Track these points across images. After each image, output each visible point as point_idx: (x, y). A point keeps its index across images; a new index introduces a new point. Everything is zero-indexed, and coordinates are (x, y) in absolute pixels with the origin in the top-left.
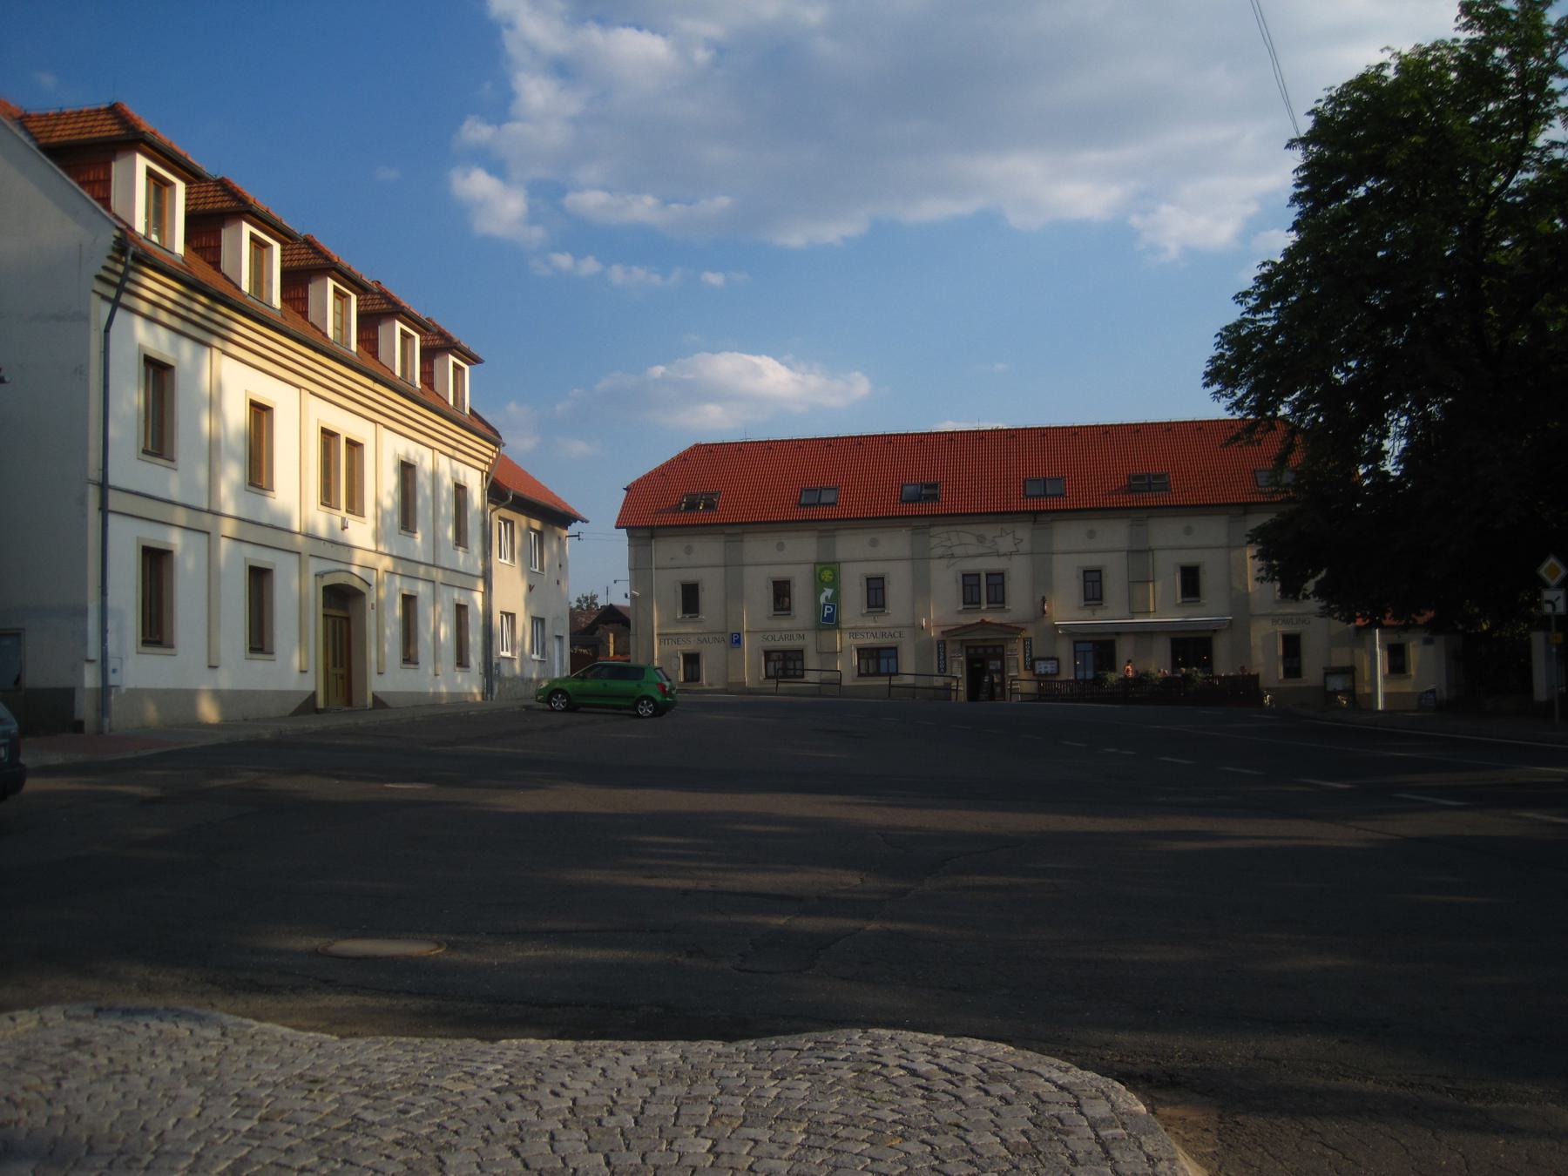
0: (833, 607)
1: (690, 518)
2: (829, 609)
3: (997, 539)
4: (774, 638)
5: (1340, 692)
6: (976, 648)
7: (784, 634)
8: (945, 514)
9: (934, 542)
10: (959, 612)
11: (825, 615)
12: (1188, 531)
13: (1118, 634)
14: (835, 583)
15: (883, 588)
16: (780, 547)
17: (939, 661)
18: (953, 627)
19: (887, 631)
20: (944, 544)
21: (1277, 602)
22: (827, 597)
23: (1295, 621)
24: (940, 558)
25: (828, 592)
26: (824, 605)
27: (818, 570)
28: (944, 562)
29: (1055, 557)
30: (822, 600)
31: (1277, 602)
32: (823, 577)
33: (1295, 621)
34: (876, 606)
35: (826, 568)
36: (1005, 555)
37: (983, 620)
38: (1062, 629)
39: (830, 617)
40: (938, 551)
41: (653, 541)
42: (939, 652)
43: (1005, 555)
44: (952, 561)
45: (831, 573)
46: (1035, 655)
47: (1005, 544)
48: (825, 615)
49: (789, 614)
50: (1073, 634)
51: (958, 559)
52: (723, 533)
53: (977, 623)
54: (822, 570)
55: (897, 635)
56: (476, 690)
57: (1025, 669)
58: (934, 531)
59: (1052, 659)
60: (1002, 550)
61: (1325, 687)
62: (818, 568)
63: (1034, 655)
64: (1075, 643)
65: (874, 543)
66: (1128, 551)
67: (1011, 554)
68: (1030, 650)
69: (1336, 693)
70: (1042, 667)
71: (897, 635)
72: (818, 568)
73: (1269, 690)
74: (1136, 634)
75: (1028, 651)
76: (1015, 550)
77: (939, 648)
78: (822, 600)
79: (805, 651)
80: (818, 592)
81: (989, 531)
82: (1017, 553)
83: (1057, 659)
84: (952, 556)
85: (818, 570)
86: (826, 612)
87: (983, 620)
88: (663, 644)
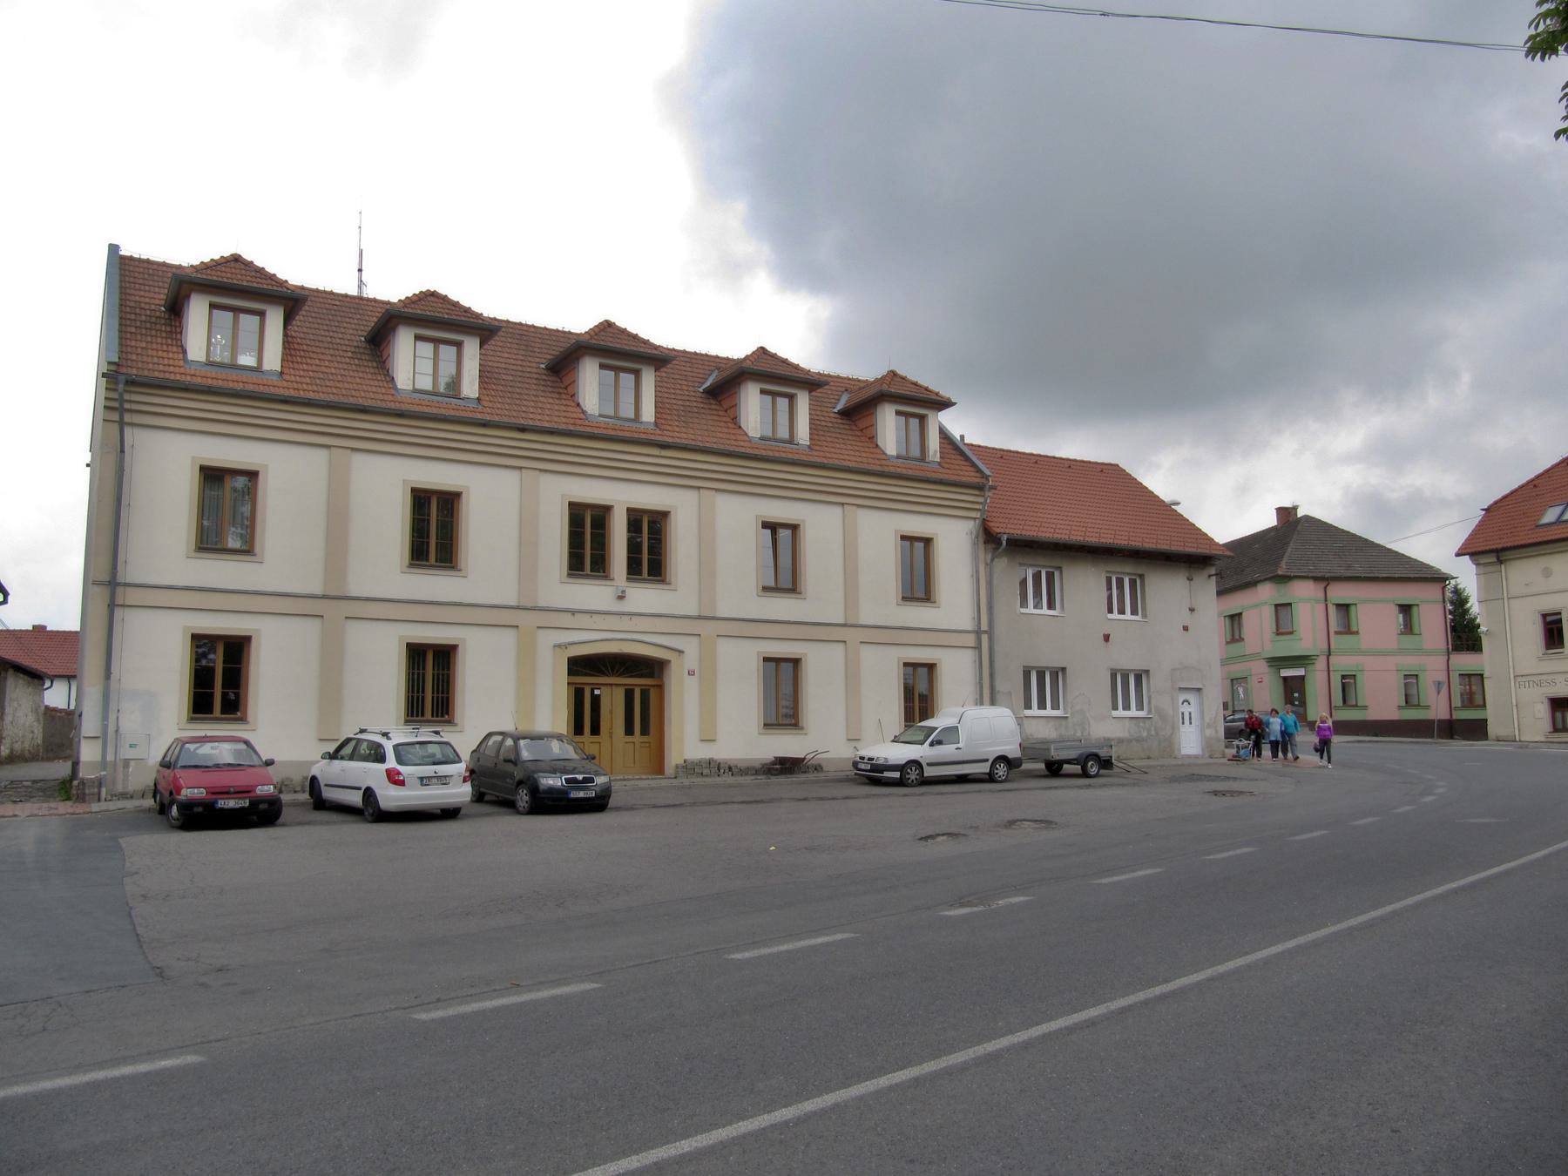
41: (1503, 566)
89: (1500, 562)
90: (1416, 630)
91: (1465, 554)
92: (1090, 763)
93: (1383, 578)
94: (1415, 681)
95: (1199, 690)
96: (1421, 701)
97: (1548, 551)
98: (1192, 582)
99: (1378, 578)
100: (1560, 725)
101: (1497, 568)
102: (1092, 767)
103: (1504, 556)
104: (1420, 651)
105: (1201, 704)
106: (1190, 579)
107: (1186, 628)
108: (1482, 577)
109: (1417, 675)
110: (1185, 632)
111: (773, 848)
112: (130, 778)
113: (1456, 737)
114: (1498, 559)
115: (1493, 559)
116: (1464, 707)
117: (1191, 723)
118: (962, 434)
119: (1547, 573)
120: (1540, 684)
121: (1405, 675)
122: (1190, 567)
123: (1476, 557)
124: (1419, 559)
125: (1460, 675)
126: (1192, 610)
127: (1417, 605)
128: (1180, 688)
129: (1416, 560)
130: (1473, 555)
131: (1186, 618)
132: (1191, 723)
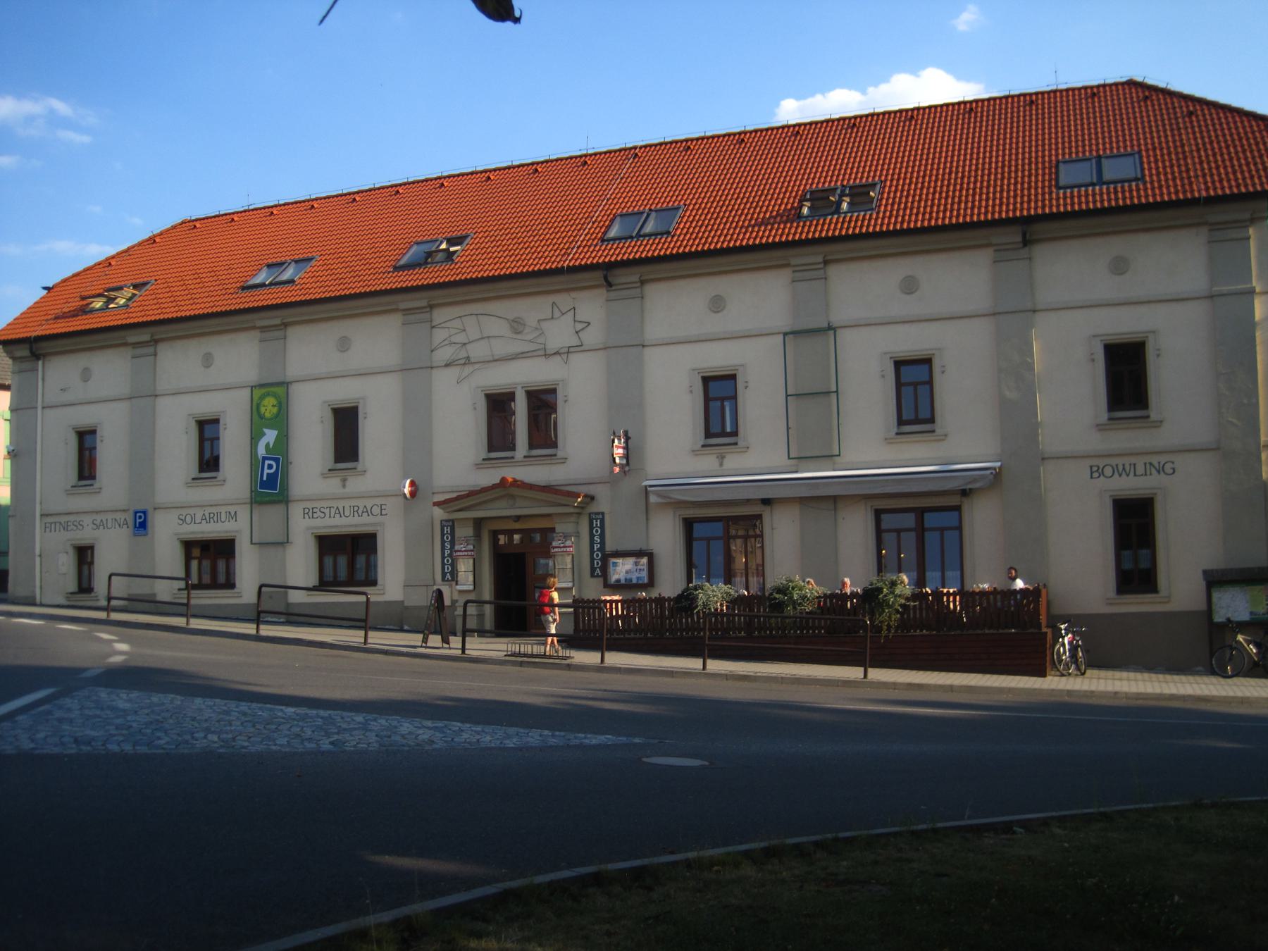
0: (277, 460)
1: (829, 226)
2: (270, 467)
3: (545, 325)
4: (340, 513)
5: (1242, 626)
6: (510, 533)
7: (208, 510)
8: (965, 223)
9: (439, 335)
10: (478, 466)
11: (265, 478)
12: (909, 286)
13: (767, 502)
14: (282, 421)
15: (930, 383)
16: (208, 360)
17: (443, 558)
18: (454, 495)
19: (361, 503)
20: (454, 339)
21: (1100, 427)
22: (267, 445)
23: (1140, 470)
24: (447, 365)
25: (270, 436)
26: (264, 459)
27: (256, 398)
28: (453, 372)
29: (647, 351)
30: (261, 451)
31: (1100, 427)
32: (263, 410)
33: (1140, 470)
34: (724, 434)
35: (268, 394)
36: (557, 353)
37: (503, 480)
38: (658, 494)
39: (271, 482)
40: (444, 354)
41: (40, 363)
42: (443, 542)
43: (557, 353)
44: (468, 369)
45: (275, 403)
46: (609, 547)
47: (559, 333)
48: (265, 478)
49: (736, 444)
50: (679, 504)
51: (477, 366)
52: (126, 344)
53: (494, 487)
54: (262, 398)
55: (376, 510)
56: (541, 572)
57: (592, 575)
58: (440, 315)
59: (638, 554)
60: (553, 345)
61: (1209, 611)
62: (257, 393)
63: (609, 547)
64: (878, 513)
65: (344, 345)
66: (785, 334)
67: (569, 351)
68: (602, 536)
69: (1233, 627)
70: (622, 569)
71: (376, 510)
72: (257, 393)
73: (1074, 621)
74: (803, 501)
75: (597, 539)
76: (575, 342)
77: (443, 535)
78: (261, 451)
79: (96, 548)
80: (255, 438)
81: (531, 309)
82: (579, 348)
83: (651, 556)
84: (468, 361)
85: (256, 398)
86: (266, 471)
87: (503, 480)
88: (48, 530)
120: (1096, 472)
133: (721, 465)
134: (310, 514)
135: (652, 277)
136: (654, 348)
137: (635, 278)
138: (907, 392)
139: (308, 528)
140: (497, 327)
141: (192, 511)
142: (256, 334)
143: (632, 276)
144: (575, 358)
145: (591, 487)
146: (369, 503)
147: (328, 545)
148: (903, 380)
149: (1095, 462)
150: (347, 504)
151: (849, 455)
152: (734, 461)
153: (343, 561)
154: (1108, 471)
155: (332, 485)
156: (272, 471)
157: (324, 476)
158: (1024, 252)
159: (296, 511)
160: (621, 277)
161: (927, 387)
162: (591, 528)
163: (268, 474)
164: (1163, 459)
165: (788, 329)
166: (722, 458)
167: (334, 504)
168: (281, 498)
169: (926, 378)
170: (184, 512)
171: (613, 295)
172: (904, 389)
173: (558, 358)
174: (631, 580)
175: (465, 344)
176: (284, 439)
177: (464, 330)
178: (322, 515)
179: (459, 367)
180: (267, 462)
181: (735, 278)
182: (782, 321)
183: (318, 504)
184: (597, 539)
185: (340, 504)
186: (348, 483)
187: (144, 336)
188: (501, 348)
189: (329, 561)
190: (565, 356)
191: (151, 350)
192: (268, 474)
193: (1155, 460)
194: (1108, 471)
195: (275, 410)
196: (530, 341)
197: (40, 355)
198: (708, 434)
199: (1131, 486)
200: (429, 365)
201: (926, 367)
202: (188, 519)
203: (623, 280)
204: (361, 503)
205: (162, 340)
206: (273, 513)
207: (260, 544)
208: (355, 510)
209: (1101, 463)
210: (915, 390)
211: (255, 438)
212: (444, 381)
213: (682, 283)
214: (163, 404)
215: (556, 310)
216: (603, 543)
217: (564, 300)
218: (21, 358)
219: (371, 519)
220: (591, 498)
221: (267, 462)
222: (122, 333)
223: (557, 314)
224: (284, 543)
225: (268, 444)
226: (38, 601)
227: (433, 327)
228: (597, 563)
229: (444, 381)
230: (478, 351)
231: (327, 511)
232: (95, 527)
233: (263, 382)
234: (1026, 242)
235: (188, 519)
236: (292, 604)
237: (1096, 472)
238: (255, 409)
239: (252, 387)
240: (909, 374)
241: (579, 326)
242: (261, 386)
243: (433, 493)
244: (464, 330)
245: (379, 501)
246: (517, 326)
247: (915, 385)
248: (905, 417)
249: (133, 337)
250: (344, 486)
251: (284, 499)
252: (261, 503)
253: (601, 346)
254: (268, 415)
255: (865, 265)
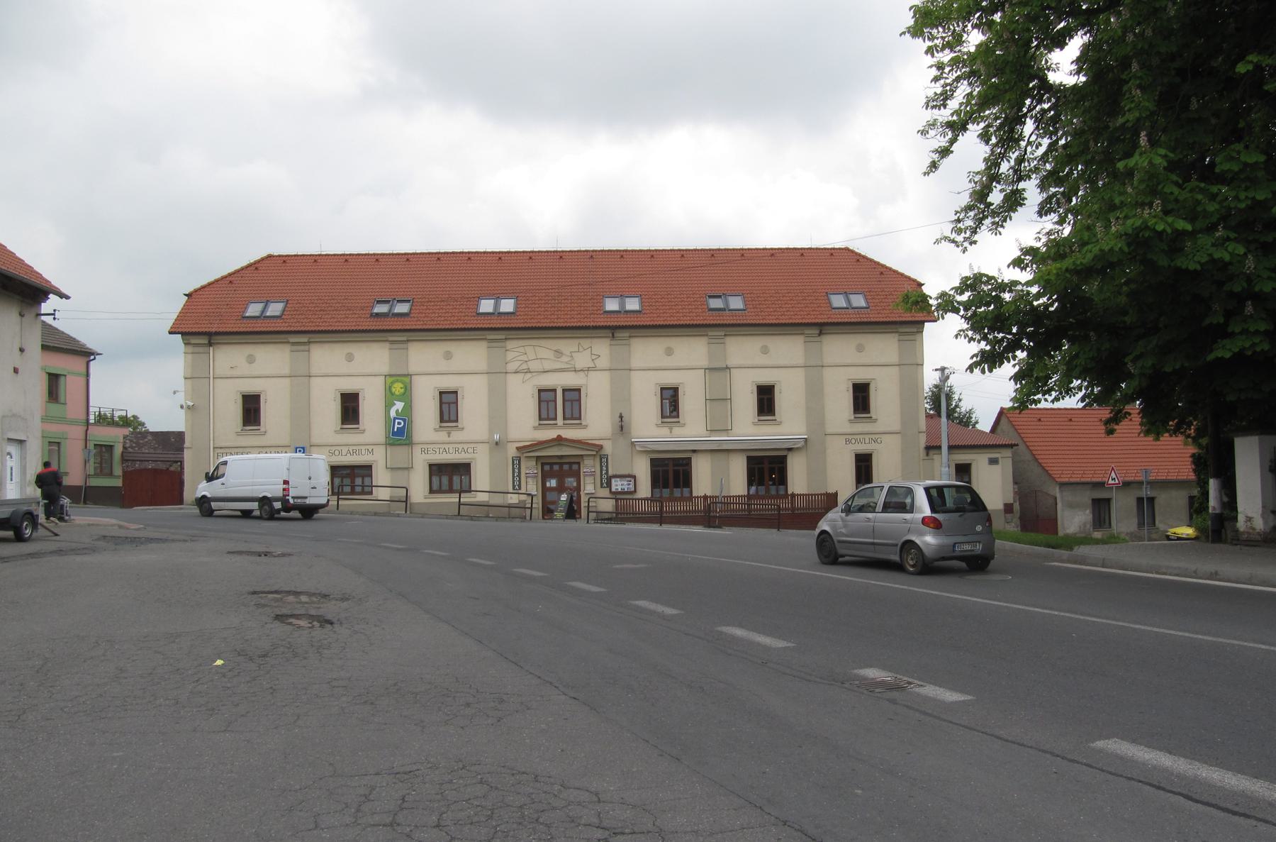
0: (404, 420)
2: (399, 423)
9: (510, 355)
10: (535, 428)
11: (396, 430)
12: (765, 350)
13: (790, 449)
14: (407, 396)
16: (350, 358)
23: (867, 441)
25: (399, 405)
26: (395, 419)
28: (520, 376)
29: (633, 373)
32: (393, 390)
33: (867, 441)
35: (397, 381)
39: (400, 432)
40: (512, 367)
41: (211, 348)
44: (529, 375)
47: (582, 360)
48: (396, 430)
52: (288, 342)
54: (393, 383)
58: (511, 344)
60: (578, 366)
62: (390, 380)
67: (589, 369)
68: (607, 467)
70: (618, 485)
75: (604, 468)
76: (592, 365)
78: (393, 414)
80: (388, 406)
82: (594, 369)
83: (634, 477)
84: (528, 371)
86: (396, 426)
89: (210, 344)
90: (62, 399)
91: (178, 333)
92: (25, 524)
93: (54, 347)
94: (57, 448)
95: (21, 442)
96: (62, 466)
97: (670, 334)
98: (24, 319)
99: (63, 348)
100: (435, 487)
101: (206, 349)
102: (26, 529)
103: (216, 339)
104: (62, 420)
105: (23, 458)
106: (22, 315)
107: (16, 371)
108: (190, 356)
109: (59, 443)
110: (15, 374)
111: (219, 662)
112: (996, 556)
113: (88, 502)
114: (209, 341)
115: (815, 331)
116: (96, 475)
117: (11, 480)
118: (925, 55)
119: (251, 360)
120: (848, 441)
121: (49, 442)
122: (22, 301)
123: (188, 337)
124: (66, 332)
125: (95, 445)
126: (22, 350)
127: (65, 376)
128: (9, 439)
129: (63, 333)
130: (183, 334)
131: (17, 360)
132: (11, 480)
133: (671, 432)
134: (426, 452)
135: (510, 337)
136: (636, 372)
137: (627, 335)
138: (544, 405)
139: (425, 460)
140: (550, 355)
141: (339, 448)
142: (387, 345)
143: (626, 334)
144: (592, 374)
145: (601, 441)
146: (465, 446)
147: (437, 470)
148: (542, 399)
149: (847, 437)
150: (451, 446)
151: (736, 430)
152: (677, 430)
153: (445, 480)
154: (853, 441)
155: (442, 436)
156: (400, 426)
157: (436, 430)
158: (818, 339)
159: (417, 450)
160: (619, 334)
161: (578, 403)
162: (601, 463)
163: (398, 428)
164: (877, 436)
165: (706, 367)
166: (671, 429)
167: (443, 446)
168: (408, 442)
169: (577, 398)
170: (334, 448)
171: (613, 342)
172: (542, 403)
173: (582, 373)
174: (617, 489)
175: (526, 361)
176: (409, 407)
177: (526, 354)
178: (434, 452)
179: (523, 374)
180: (397, 421)
181: (678, 339)
182: (385, 369)
183: (432, 446)
184: (604, 468)
185: (446, 447)
186: (451, 435)
187: (304, 339)
188: (548, 366)
189: (436, 479)
190: (586, 372)
191: (306, 348)
192: (398, 428)
193: (873, 437)
194: (853, 441)
195: (402, 390)
196: (566, 363)
197: (214, 343)
198: (442, 420)
199: (863, 448)
200: (820, 364)
201: (455, 395)
202: (337, 453)
203: (621, 335)
204: (460, 446)
205: (633, 337)
206: (401, 452)
207: (392, 469)
208: (457, 450)
209: (850, 437)
210: (449, 405)
211: (388, 406)
212: (514, 382)
213: (463, 343)
214: (827, 373)
215: (580, 348)
216: (607, 470)
217: (586, 343)
218: (194, 344)
219: (467, 456)
220: (601, 447)
221: (397, 421)
222: (286, 336)
223: (581, 349)
224: (408, 469)
225: (397, 410)
226: (954, 489)
227: (506, 350)
228: (605, 481)
229: (514, 382)
230: (534, 366)
231: (438, 451)
232: (331, 454)
233: (392, 373)
234: (820, 334)
235: (337, 453)
236: (414, 503)
237: (848, 441)
238: (389, 391)
239: (386, 376)
240: (446, 398)
241: (594, 357)
242: (391, 376)
243: (311, 446)
244: (526, 354)
245: (472, 445)
246: (559, 353)
247: (572, 401)
248: (542, 417)
249: (293, 339)
250: (449, 436)
251: (410, 443)
252: (391, 445)
253: (897, 363)
254: (397, 393)
255: (744, 338)
